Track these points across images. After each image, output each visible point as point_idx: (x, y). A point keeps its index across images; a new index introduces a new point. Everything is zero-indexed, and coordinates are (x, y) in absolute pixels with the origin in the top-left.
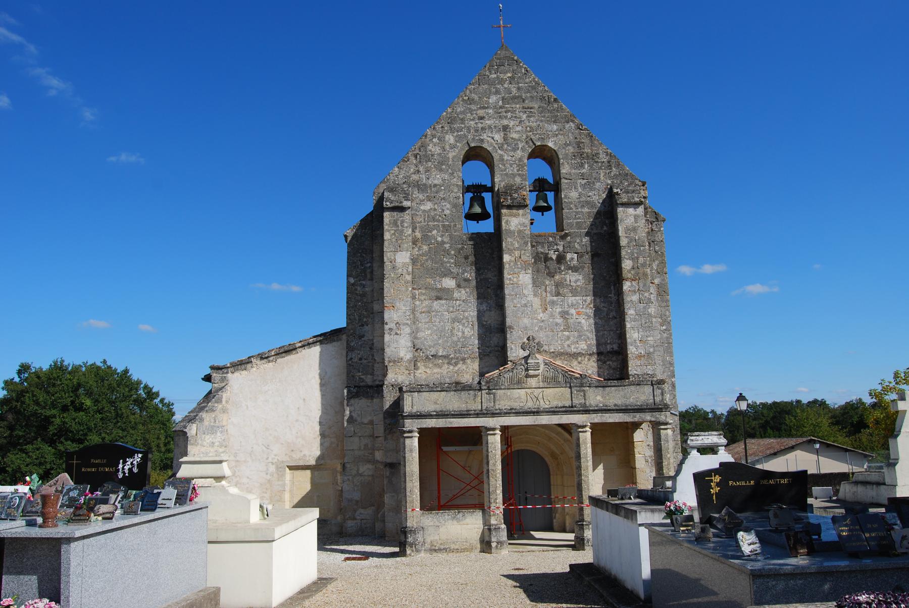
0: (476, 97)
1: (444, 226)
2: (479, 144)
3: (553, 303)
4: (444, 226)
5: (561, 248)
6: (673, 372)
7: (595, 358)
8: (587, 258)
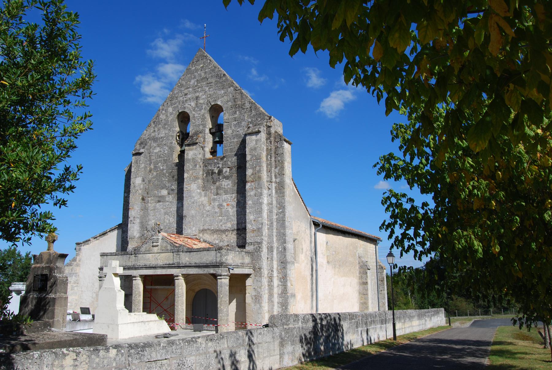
0: (184, 83)
1: (164, 160)
2: (183, 110)
3: (214, 200)
4: (164, 160)
5: (221, 166)
6: (285, 240)
7: (235, 232)
8: (234, 170)
